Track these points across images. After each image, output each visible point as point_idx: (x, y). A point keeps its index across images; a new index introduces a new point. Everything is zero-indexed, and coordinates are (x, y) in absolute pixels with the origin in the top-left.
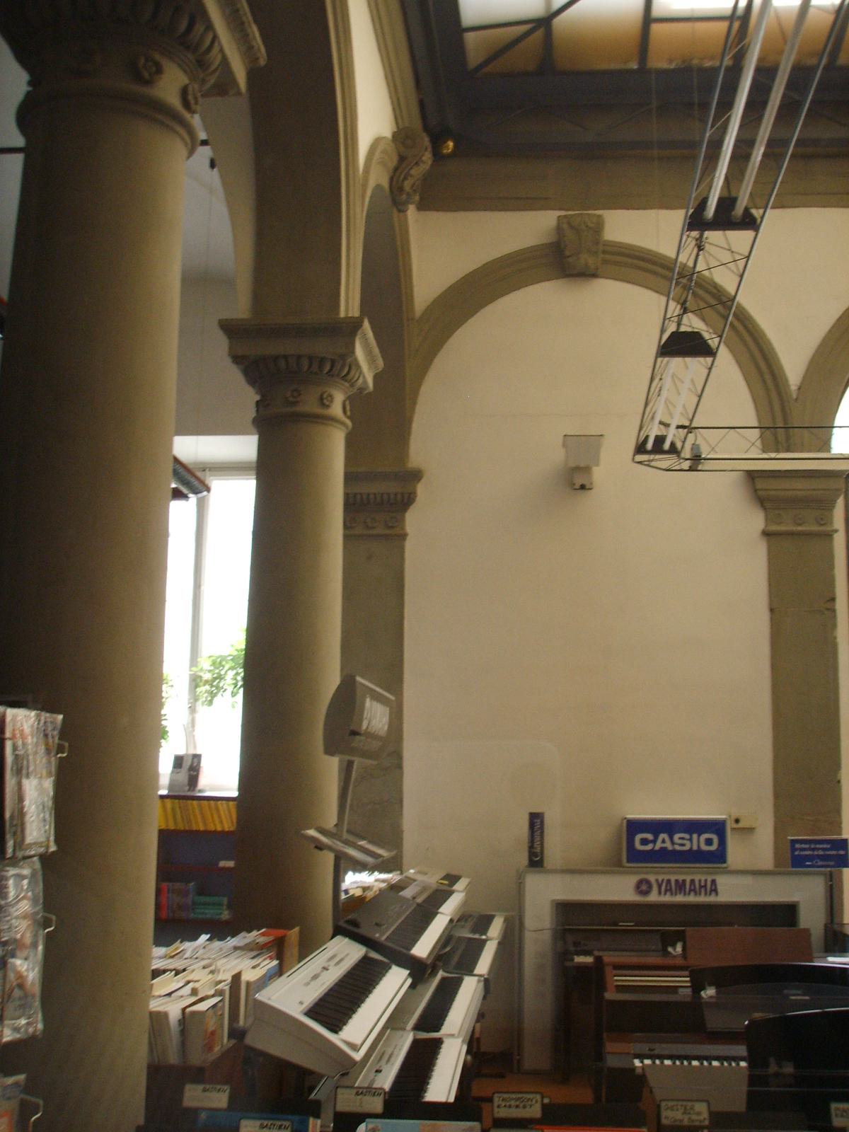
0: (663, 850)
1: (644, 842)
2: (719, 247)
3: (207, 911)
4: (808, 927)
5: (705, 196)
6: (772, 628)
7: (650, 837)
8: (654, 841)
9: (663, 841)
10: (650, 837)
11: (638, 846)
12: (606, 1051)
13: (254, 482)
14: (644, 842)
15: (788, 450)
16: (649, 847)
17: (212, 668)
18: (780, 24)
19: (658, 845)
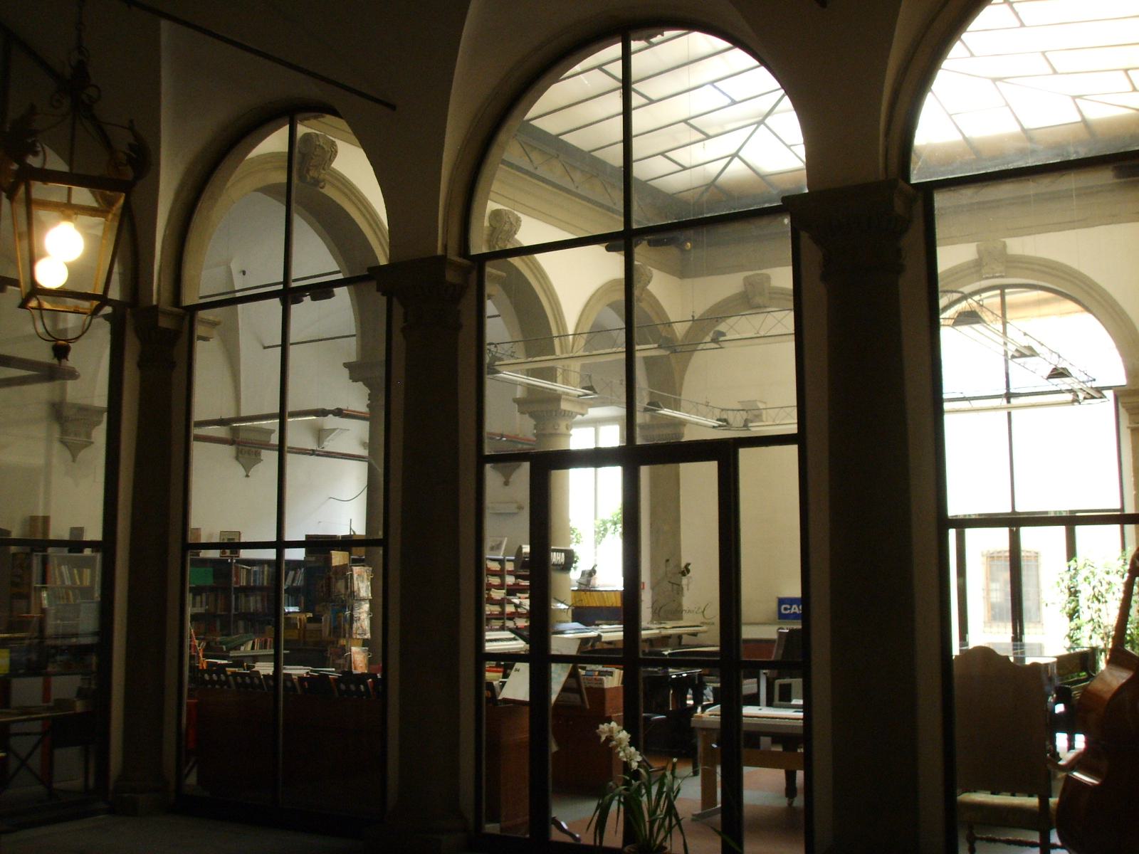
0: (795, 613)
1: (786, 609)
2: (321, 340)
3: (657, 631)
4: (9, 529)
5: (14, 204)
6: (540, 220)
7: (788, 607)
8: (790, 609)
9: (795, 609)
10: (788, 607)
11: (783, 611)
12: (506, 156)
13: (242, 550)
14: (786, 609)
15: (567, 385)
16: (788, 612)
17: (1072, 598)
18: (551, 435)
19: (793, 611)
